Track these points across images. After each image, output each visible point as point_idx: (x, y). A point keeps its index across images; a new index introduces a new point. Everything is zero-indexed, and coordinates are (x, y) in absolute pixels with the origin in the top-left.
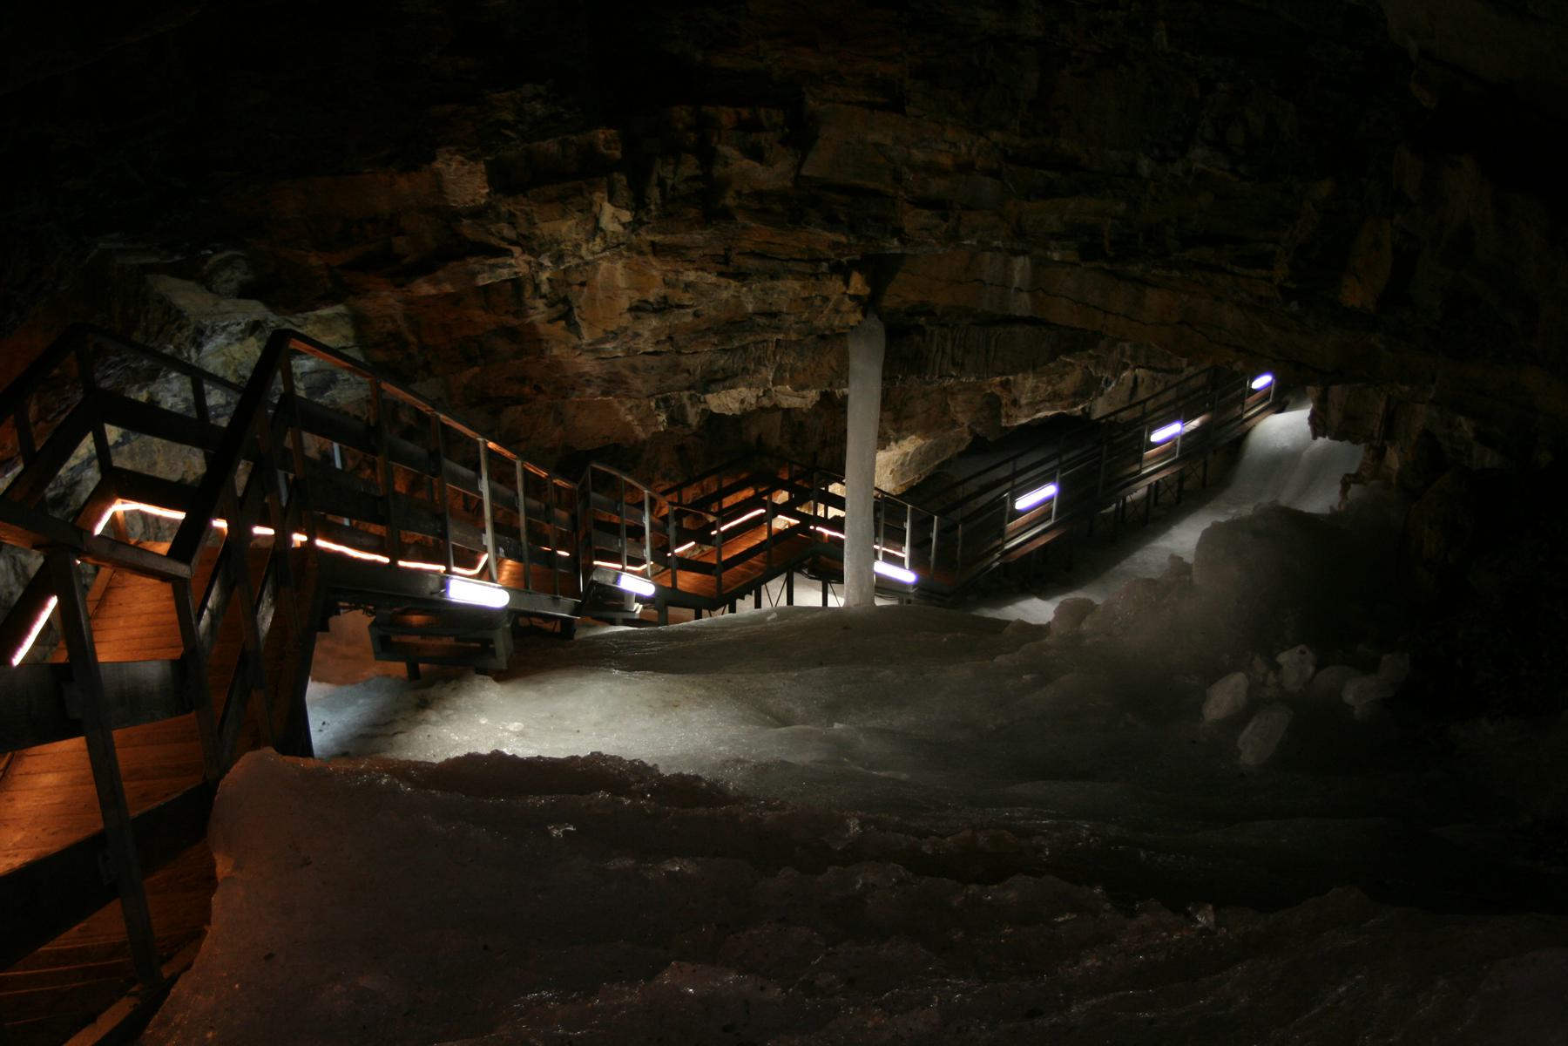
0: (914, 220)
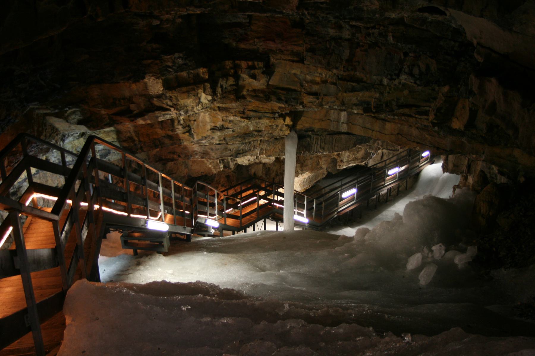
0: (307, 99)
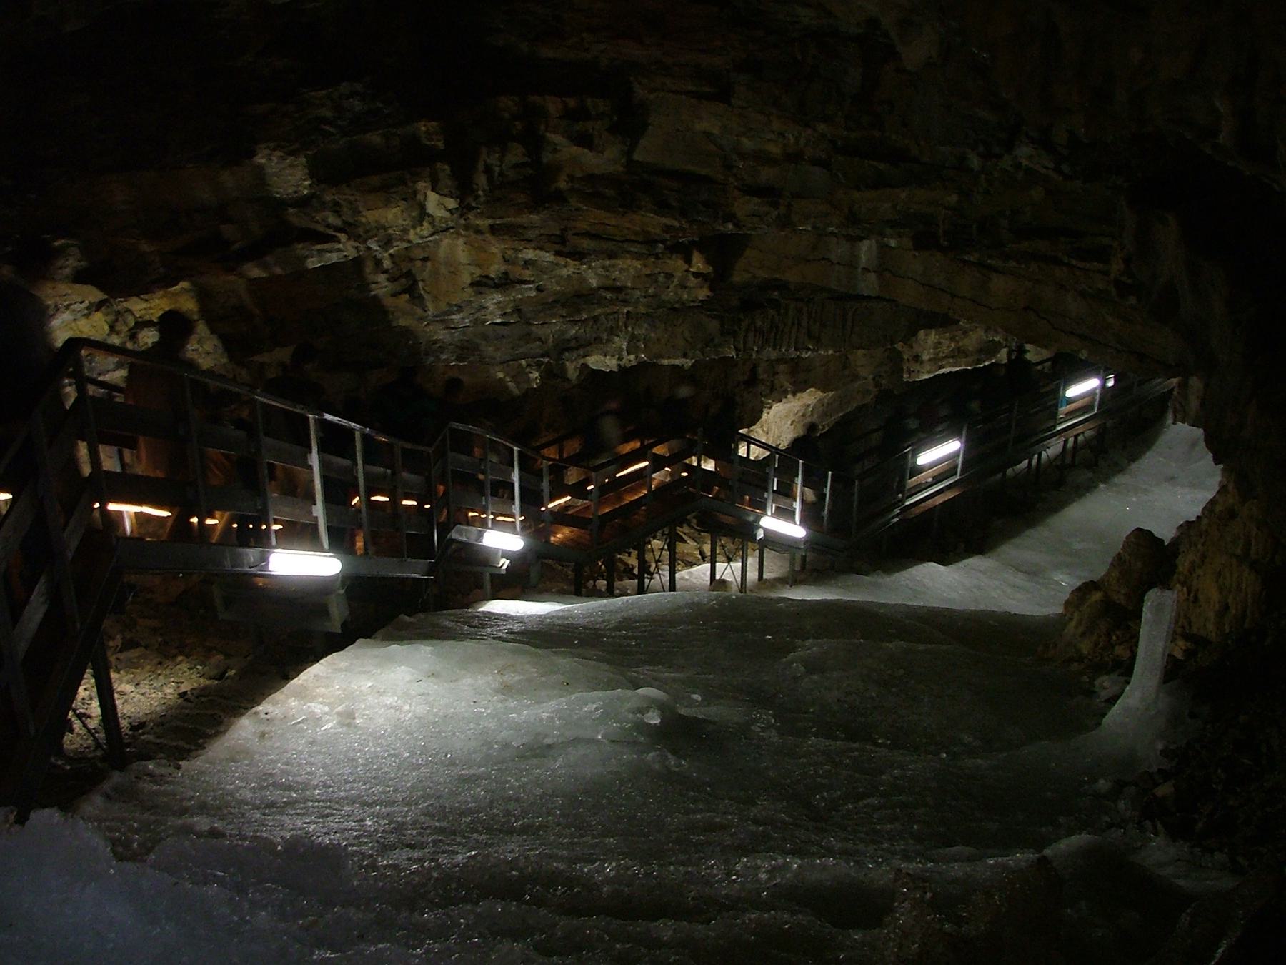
0: (745, 206)
